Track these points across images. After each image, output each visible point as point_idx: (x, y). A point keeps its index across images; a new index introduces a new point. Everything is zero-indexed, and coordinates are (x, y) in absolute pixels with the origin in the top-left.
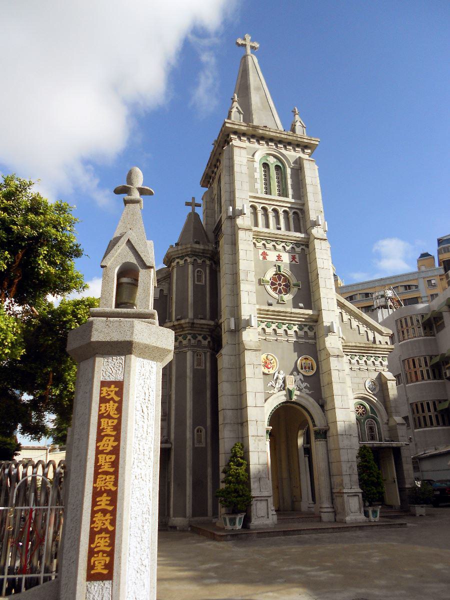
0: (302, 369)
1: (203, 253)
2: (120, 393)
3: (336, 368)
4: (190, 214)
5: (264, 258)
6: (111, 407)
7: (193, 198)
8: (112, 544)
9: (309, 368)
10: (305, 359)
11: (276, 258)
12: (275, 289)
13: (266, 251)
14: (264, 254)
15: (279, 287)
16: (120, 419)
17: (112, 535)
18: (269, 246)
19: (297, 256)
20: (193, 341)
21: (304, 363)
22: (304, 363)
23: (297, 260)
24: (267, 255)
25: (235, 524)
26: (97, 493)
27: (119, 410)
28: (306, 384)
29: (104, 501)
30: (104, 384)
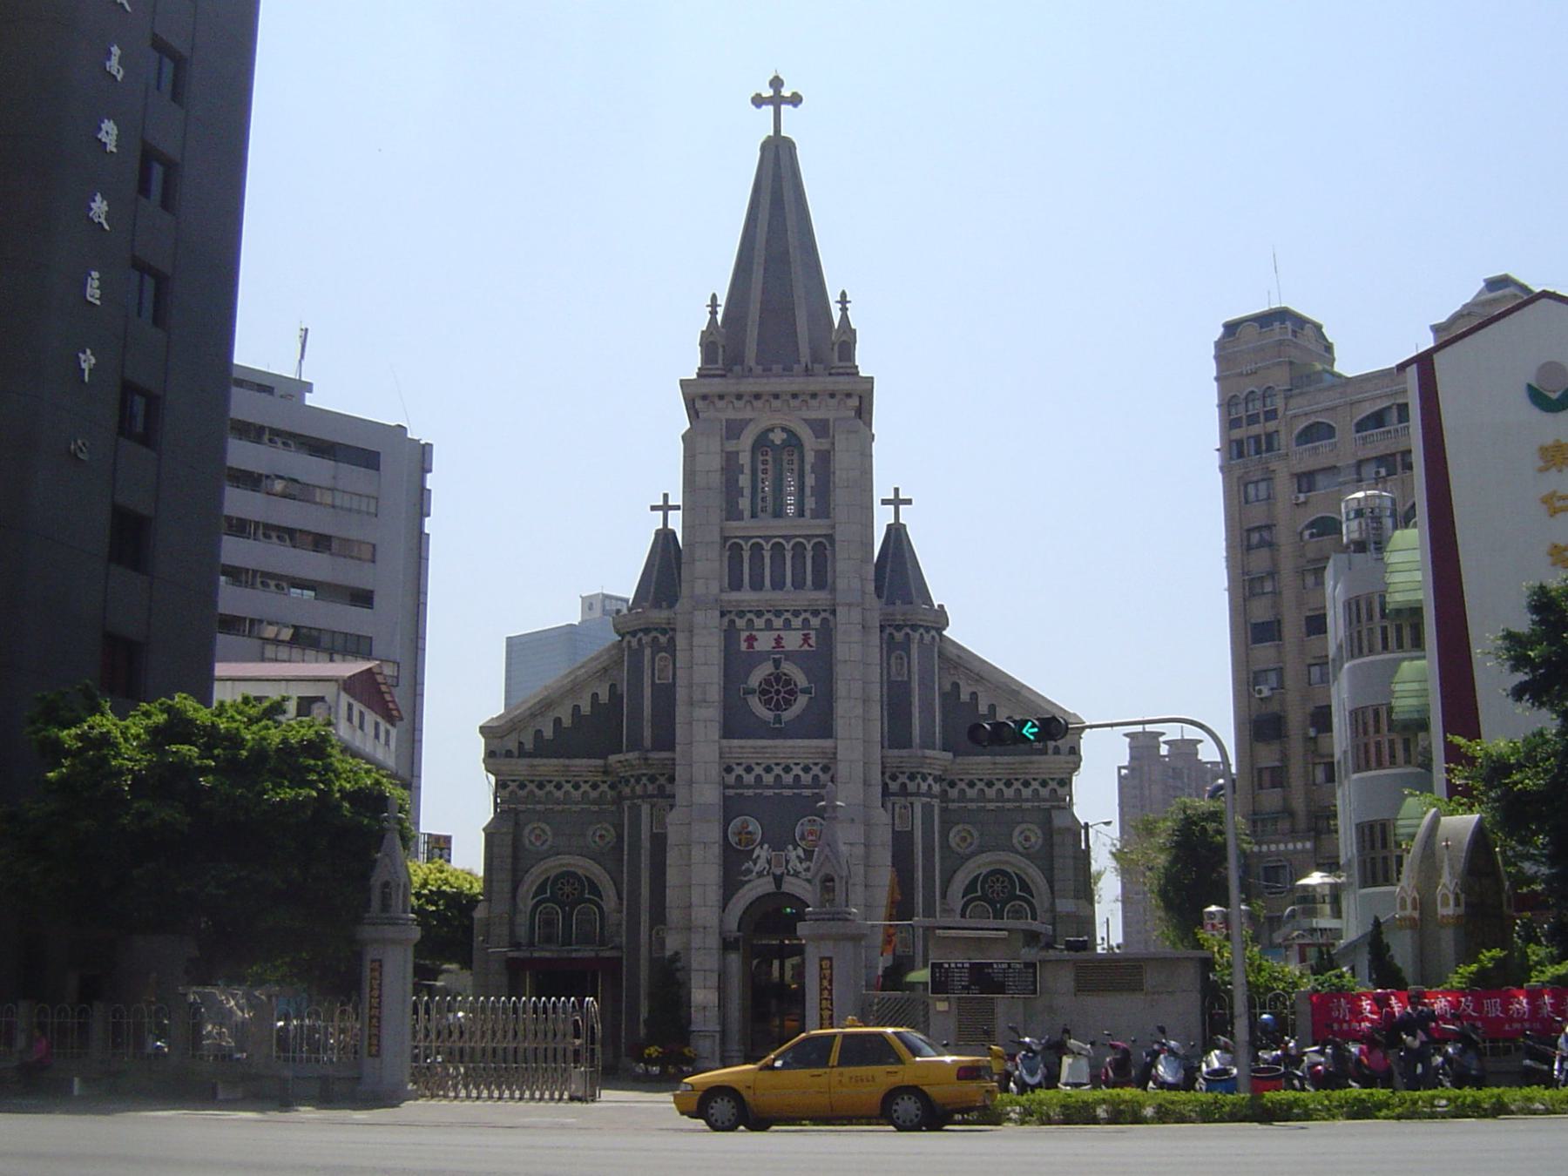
1: (669, 624)
2: (381, 966)
4: (658, 533)
5: (751, 646)
6: (376, 974)
7: (666, 496)
8: (379, 1041)
11: (774, 644)
12: (767, 703)
13: (754, 633)
14: (751, 640)
15: (775, 697)
16: (381, 980)
17: (379, 1036)
18: (759, 623)
19: (813, 633)
20: (650, 787)
23: (812, 641)
24: (756, 640)
26: (371, 1018)
27: (381, 974)
29: (374, 1021)
30: (373, 961)
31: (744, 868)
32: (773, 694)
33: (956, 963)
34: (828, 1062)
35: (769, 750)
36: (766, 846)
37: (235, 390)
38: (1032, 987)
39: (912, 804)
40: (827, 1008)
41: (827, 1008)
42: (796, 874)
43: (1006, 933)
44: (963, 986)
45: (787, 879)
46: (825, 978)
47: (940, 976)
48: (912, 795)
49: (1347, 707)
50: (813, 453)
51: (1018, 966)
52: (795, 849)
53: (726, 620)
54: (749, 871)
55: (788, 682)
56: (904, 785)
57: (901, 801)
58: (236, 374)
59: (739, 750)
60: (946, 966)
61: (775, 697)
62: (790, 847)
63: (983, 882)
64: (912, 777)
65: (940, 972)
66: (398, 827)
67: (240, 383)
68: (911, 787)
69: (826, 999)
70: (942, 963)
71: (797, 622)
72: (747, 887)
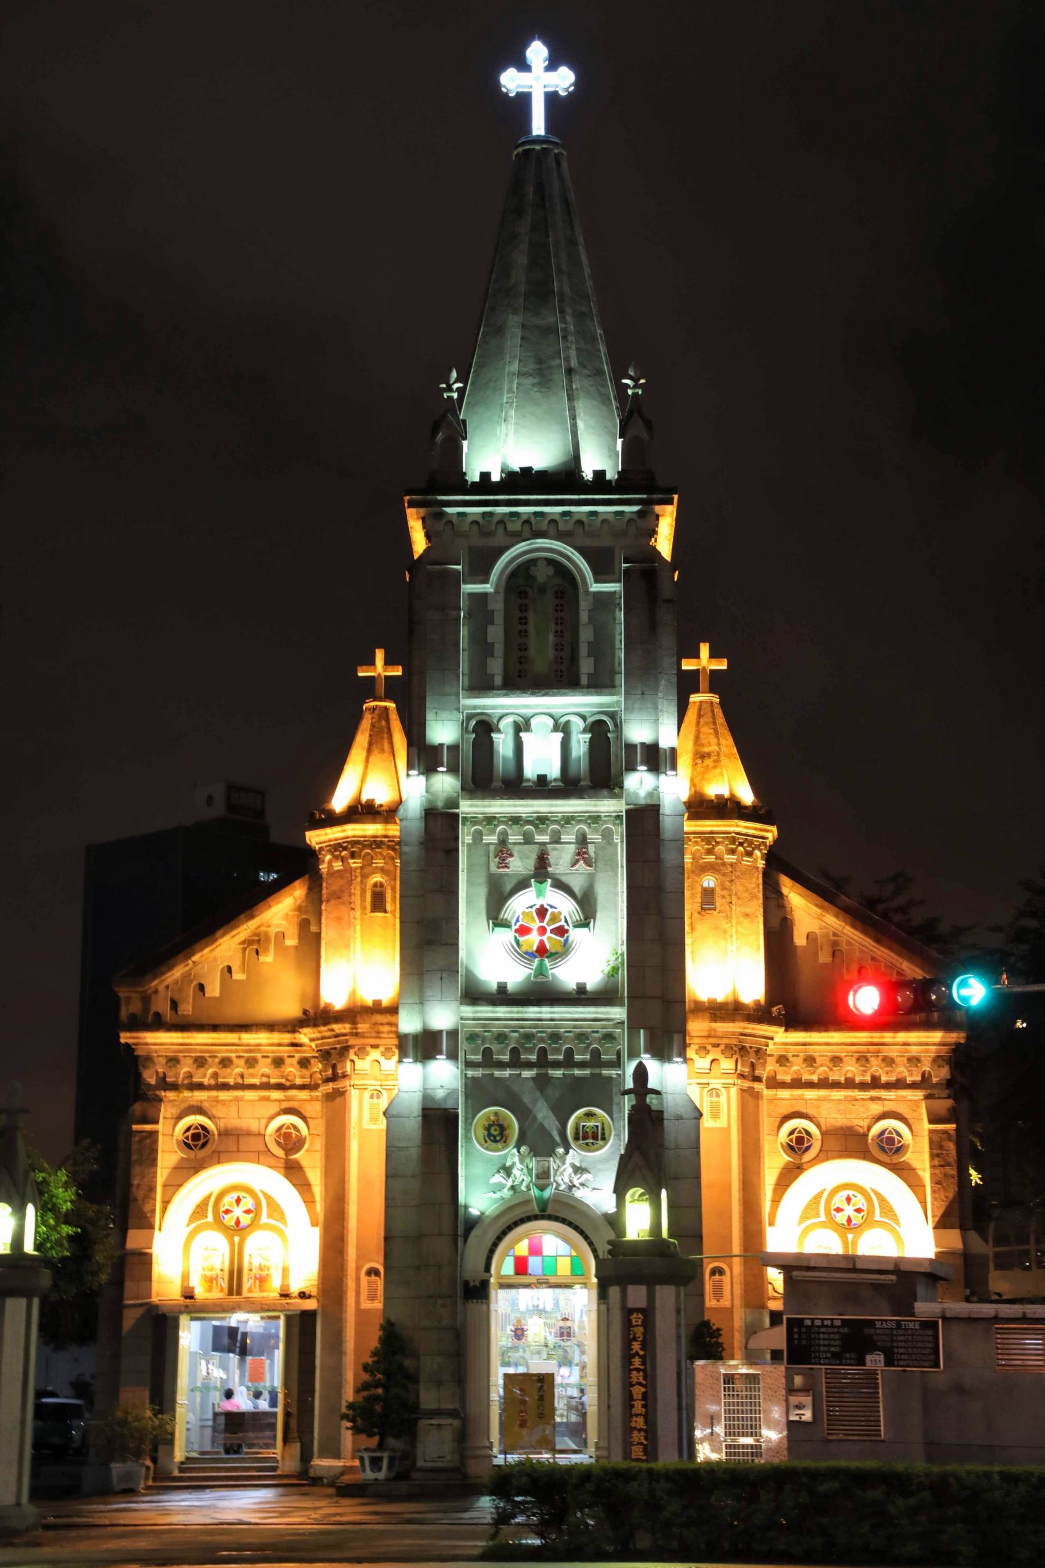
9: (595, 1137)
25: (380, 1469)
32: (549, 929)
33: (822, 1320)
38: (932, 1357)
40: (640, 1384)
41: (640, 1384)
43: (893, 1277)
44: (832, 1352)
46: (635, 1339)
47: (800, 1339)
49: (731, 1081)
50: (495, 655)
51: (911, 1326)
60: (808, 1323)
63: (828, 1201)
65: (800, 1333)
66: (409, 1023)
69: (638, 1370)
70: (803, 1319)
71: (569, 837)
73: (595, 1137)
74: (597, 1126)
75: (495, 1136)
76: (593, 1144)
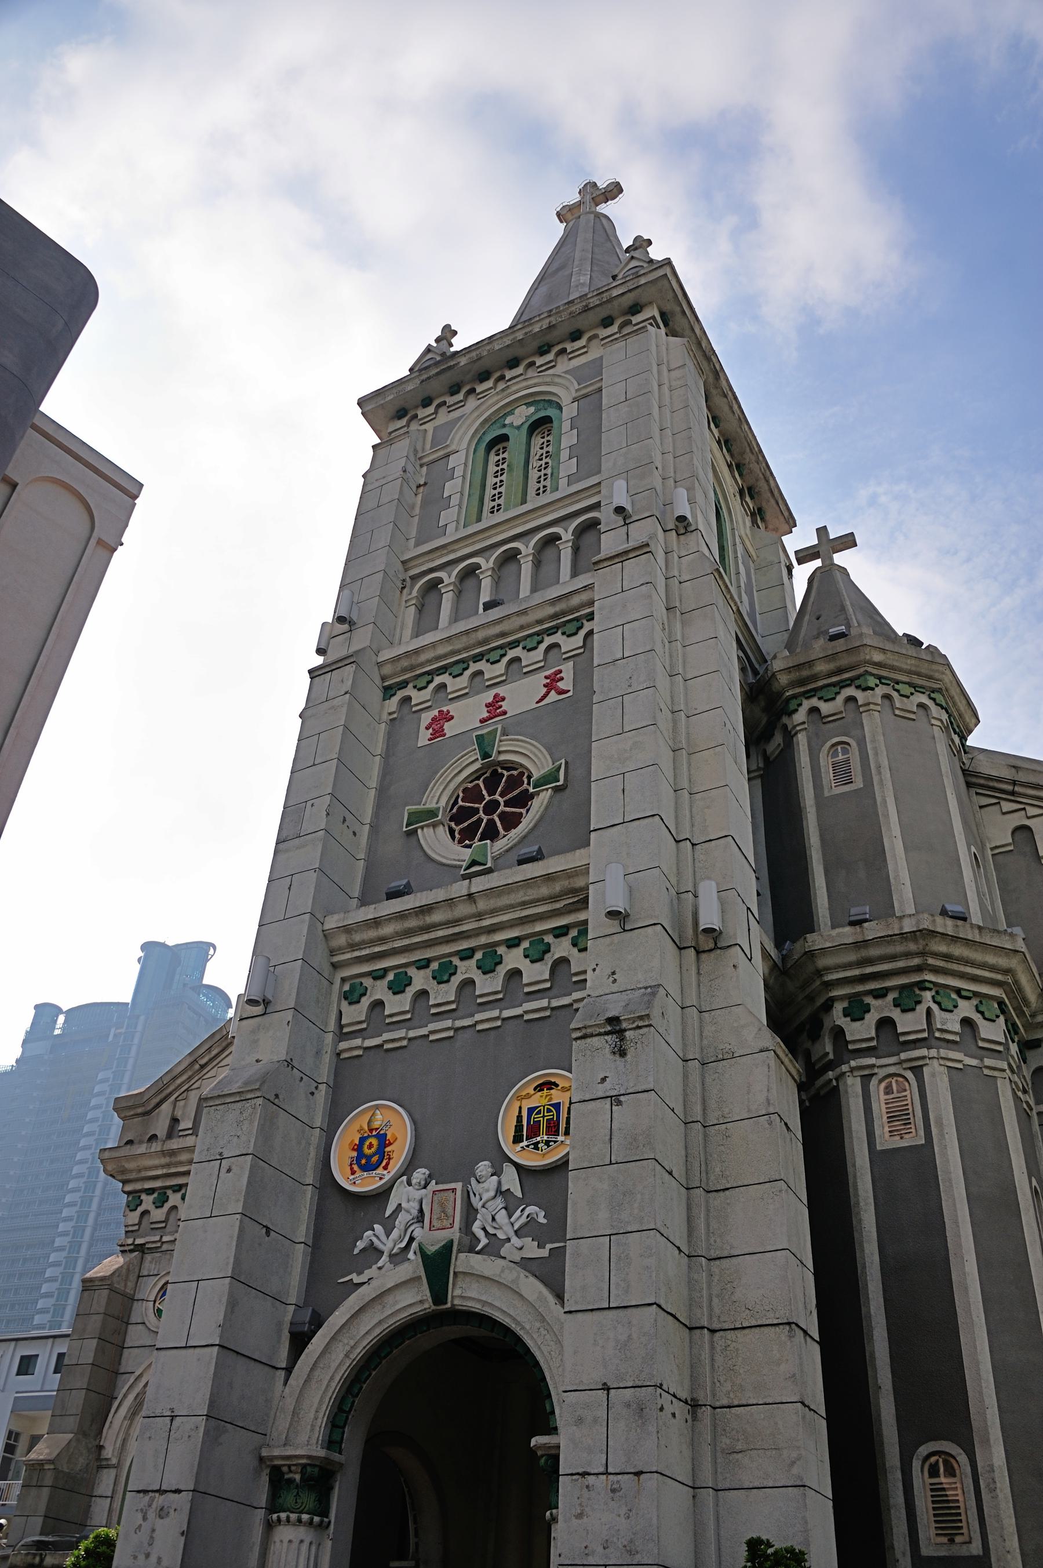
0: (517, 1139)
3: (600, 1091)
5: (438, 733)
10: (539, 1088)
21: (531, 1110)
22: (531, 1110)
28: (531, 1209)
31: (360, 1245)
34: (7, 1477)
35: (437, 917)
36: (420, 1174)
37: (30, 431)
39: (918, 1071)
42: (494, 1248)
45: (462, 1262)
48: (916, 1044)
52: (497, 1172)
53: (393, 703)
54: (373, 1252)
55: (470, 794)
56: (886, 1024)
57: (886, 1064)
58: (37, 420)
59: (372, 934)
61: (485, 818)
62: (483, 1167)
64: (907, 999)
67: (35, 428)
68: (908, 1023)
72: (353, 1302)
73: (553, 1128)
74: (557, 1106)
75: (369, 1158)
76: (547, 1143)
